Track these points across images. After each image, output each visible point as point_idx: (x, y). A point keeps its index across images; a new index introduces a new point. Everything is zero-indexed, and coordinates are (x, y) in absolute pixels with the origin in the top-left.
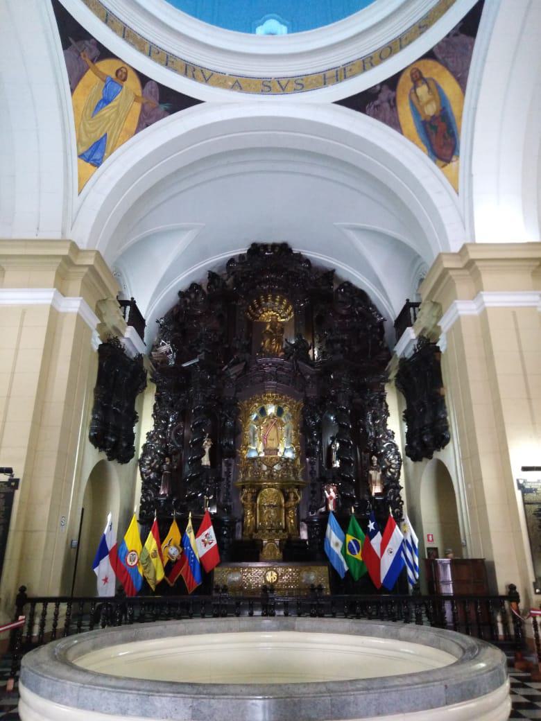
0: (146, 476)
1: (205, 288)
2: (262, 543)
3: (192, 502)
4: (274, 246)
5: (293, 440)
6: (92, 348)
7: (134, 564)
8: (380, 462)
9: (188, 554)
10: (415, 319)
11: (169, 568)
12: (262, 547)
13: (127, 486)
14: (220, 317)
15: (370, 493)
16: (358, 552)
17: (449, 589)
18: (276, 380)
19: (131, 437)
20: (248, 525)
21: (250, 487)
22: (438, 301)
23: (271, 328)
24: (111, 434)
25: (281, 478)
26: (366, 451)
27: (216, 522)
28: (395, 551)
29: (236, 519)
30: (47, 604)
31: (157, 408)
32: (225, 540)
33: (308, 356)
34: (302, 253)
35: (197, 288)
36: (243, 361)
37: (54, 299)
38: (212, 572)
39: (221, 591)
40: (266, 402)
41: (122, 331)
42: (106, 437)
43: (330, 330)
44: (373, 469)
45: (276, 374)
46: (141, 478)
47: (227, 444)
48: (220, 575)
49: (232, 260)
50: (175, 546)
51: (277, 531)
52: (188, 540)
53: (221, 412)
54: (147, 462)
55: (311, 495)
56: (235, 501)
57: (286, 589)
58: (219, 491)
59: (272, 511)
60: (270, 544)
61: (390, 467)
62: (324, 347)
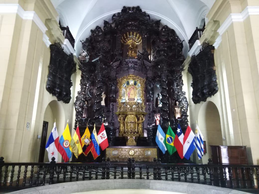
0: (77, 110)
1: (102, 28)
2: (128, 138)
3: (97, 120)
4: (133, 8)
5: (141, 95)
6: (46, 46)
7: (67, 146)
8: (179, 104)
9: (94, 142)
10: (200, 36)
11: (85, 148)
12: (127, 140)
13: (68, 113)
14: (109, 41)
15: (175, 117)
16: (172, 142)
17: (225, 160)
18: (134, 69)
19: (69, 93)
20: (121, 131)
21: (122, 115)
22: (217, 20)
23: (131, 46)
24: (58, 87)
25: (136, 111)
26: (173, 100)
27: (107, 129)
28: (191, 142)
29: (116, 128)
30: (21, 166)
31: (82, 81)
32: (111, 137)
33: (149, 58)
34: (146, 12)
35: (99, 29)
36: (120, 60)
37: (18, 10)
38: (105, 151)
39: (106, 160)
40: (129, 79)
41: (63, 42)
42: (55, 89)
43: (158, 47)
44: (176, 107)
45: (134, 67)
46: (75, 111)
47: (112, 96)
48: (109, 151)
49: (114, 15)
50: (88, 138)
51: (134, 133)
52: (94, 136)
53: (110, 83)
54: (78, 104)
55: (149, 118)
56: (116, 120)
57: (138, 158)
58: (109, 116)
59: (132, 124)
60: (131, 139)
61: (183, 107)
62: (155, 55)
